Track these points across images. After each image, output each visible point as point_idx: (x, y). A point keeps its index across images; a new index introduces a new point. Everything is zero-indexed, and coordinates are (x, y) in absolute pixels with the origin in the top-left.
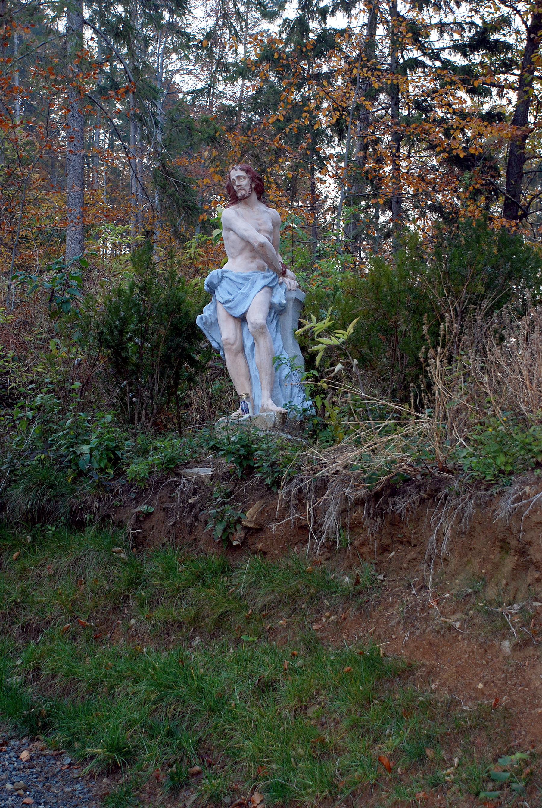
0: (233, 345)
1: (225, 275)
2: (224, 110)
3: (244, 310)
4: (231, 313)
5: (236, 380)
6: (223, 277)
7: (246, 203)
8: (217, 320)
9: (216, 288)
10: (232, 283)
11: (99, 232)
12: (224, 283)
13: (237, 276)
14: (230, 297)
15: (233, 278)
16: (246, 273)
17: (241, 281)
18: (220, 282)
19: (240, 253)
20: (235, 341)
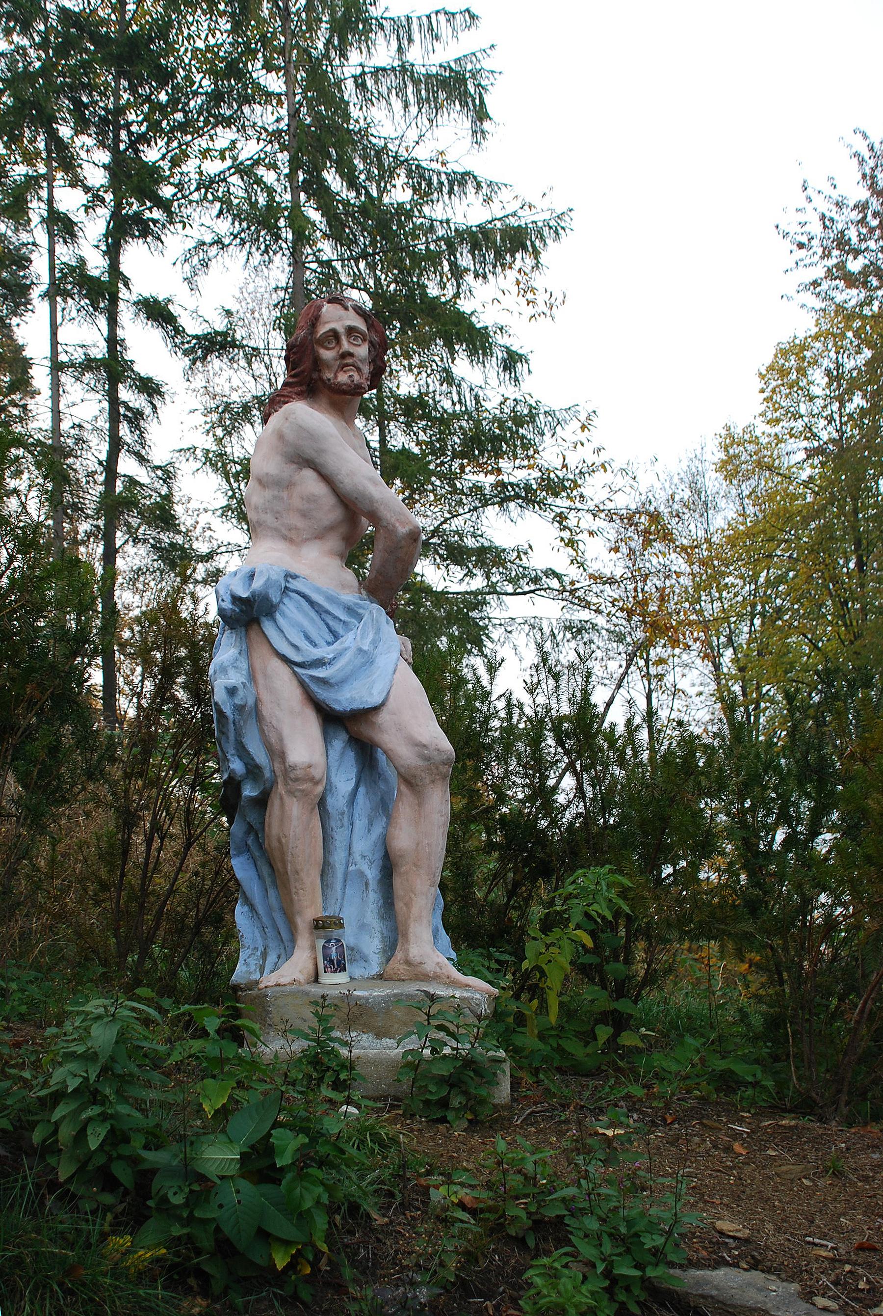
4: (322, 694)
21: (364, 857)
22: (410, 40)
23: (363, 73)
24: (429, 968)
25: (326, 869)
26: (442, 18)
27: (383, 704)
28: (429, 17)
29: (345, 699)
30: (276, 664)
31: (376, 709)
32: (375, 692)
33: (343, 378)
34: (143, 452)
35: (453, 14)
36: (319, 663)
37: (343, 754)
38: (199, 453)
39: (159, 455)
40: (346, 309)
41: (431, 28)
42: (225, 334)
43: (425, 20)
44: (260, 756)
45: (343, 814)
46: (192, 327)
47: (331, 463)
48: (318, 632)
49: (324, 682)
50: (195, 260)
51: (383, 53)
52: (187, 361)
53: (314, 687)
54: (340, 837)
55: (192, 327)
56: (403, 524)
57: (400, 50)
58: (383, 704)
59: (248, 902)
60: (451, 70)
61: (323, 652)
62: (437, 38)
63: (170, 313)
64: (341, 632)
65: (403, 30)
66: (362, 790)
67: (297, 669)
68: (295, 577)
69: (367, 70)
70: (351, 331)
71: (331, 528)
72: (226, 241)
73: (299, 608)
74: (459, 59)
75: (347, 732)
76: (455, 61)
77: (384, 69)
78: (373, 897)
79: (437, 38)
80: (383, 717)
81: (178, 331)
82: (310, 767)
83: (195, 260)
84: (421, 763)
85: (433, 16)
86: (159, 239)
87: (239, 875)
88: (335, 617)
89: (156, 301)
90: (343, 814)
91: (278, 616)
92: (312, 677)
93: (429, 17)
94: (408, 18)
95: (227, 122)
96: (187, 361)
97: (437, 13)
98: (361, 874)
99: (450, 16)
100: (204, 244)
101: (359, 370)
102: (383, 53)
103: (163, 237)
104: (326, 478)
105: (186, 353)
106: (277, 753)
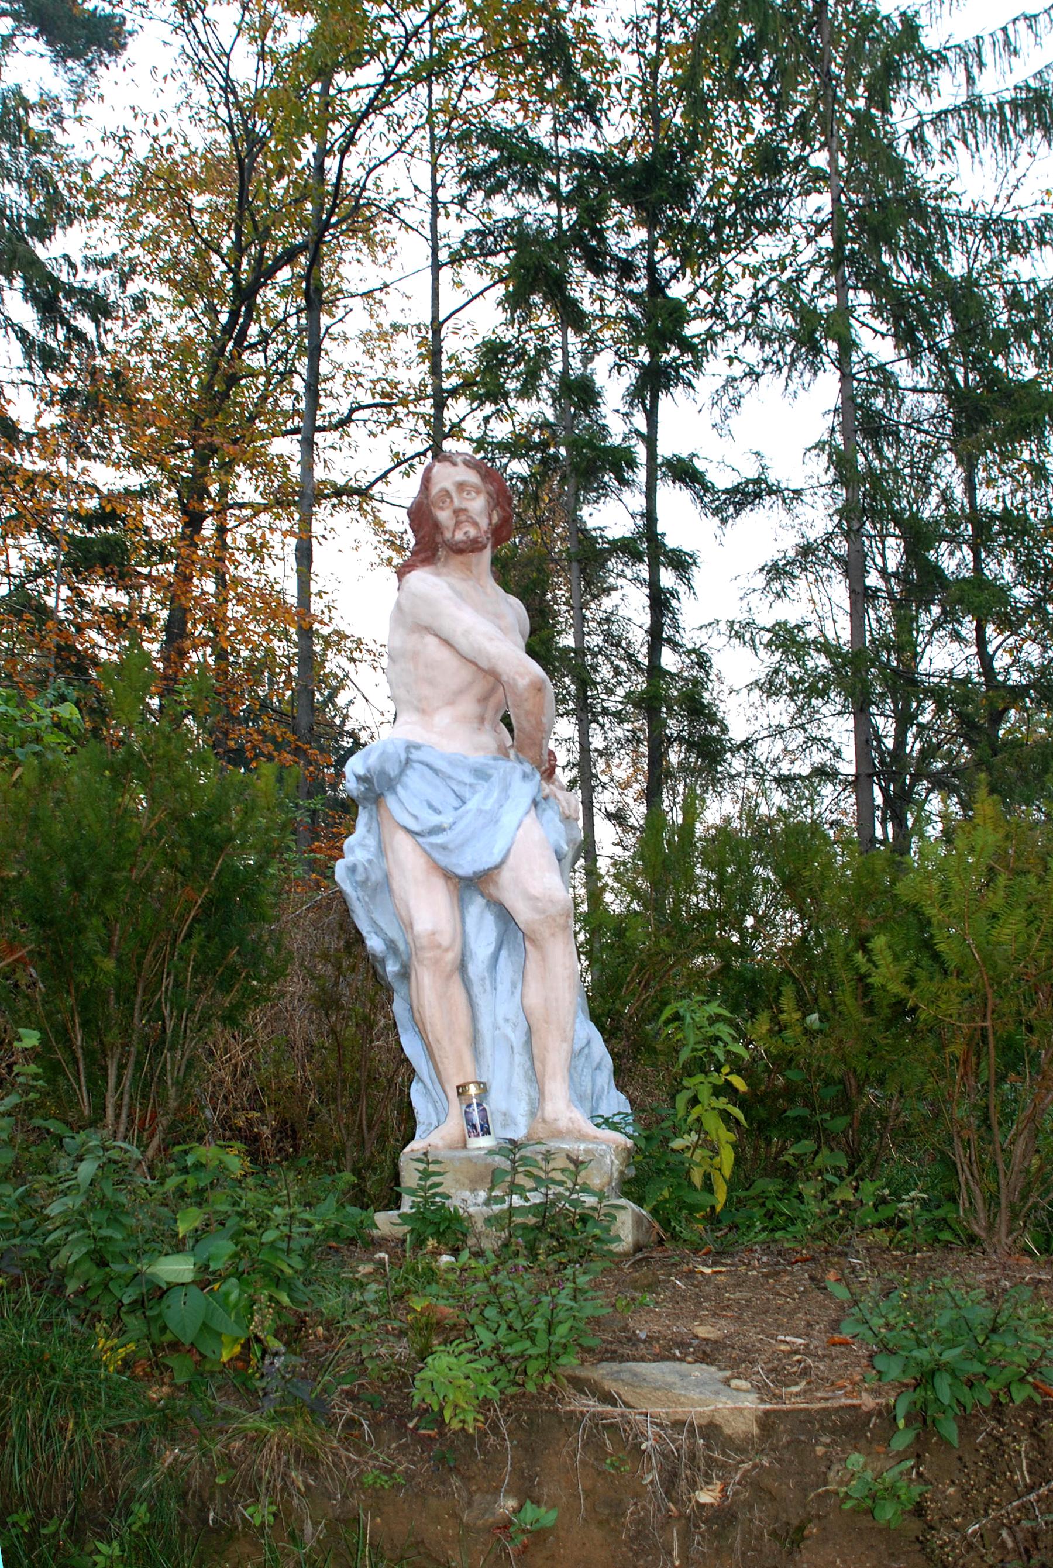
0: (447, 950)
1: (415, 755)
2: (206, 819)
3: (496, 859)
4: (443, 860)
5: (445, 1043)
6: (408, 761)
7: (468, 567)
8: (387, 877)
9: (392, 789)
10: (437, 781)
11: (258, 1471)
12: (414, 779)
13: (451, 763)
14: (435, 820)
15: (440, 764)
16: (478, 758)
17: (468, 778)
18: (402, 772)
19: (451, 703)
20: (454, 940)
21: (507, 1020)
22: (981, 65)
23: (921, 124)
24: (563, 1124)
25: (475, 1039)
26: (1022, 25)
27: (503, 862)
28: (1004, 30)
29: (467, 865)
30: (401, 837)
31: (498, 867)
32: (496, 851)
33: (459, 536)
34: (678, 638)
35: (1035, 16)
36: (438, 830)
37: (481, 917)
38: (723, 627)
39: (689, 638)
40: (455, 464)
41: (1007, 42)
42: (757, 481)
43: (1000, 35)
44: (393, 933)
45: (483, 979)
46: (722, 480)
47: (446, 626)
48: (443, 797)
49: (444, 847)
50: (725, 400)
51: (950, 88)
52: (716, 520)
53: (436, 855)
54: (483, 1003)
55: (722, 480)
56: (522, 676)
57: (970, 80)
58: (503, 862)
59: (420, 1080)
60: (1028, 89)
61: (445, 819)
62: (1016, 53)
63: (696, 471)
64: (467, 795)
65: (972, 56)
66: (504, 953)
67: (420, 839)
68: (418, 747)
69: (926, 118)
70: (461, 486)
71: (460, 692)
72: (758, 370)
73: (422, 776)
74: (1040, 72)
75: (483, 895)
76: (1034, 77)
77: (946, 112)
78: (520, 1058)
79: (1016, 53)
80: (506, 876)
81: (708, 488)
82: (434, 933)
83: (725, 400)
84: (537, 917)
85: (1010, 27)
86: (690, 385)
87: (409, 1051)
88: (460, 782)
89: (680, 460)
90: (483, 979)
91: (399, 789)
92: (432, 845)
93: (1004, 30)
94: (978, 39)
95: (770, 227)
96: (716, 520)
97: (1014, 21)
98: (507, 1038)
99: (1031, 19)
100: (734, 379)
101: (475, 524)
102: (950, 88)
103: (694, 382)
104: (447, 643)
105: (716, 512)
106: (407, 926)
